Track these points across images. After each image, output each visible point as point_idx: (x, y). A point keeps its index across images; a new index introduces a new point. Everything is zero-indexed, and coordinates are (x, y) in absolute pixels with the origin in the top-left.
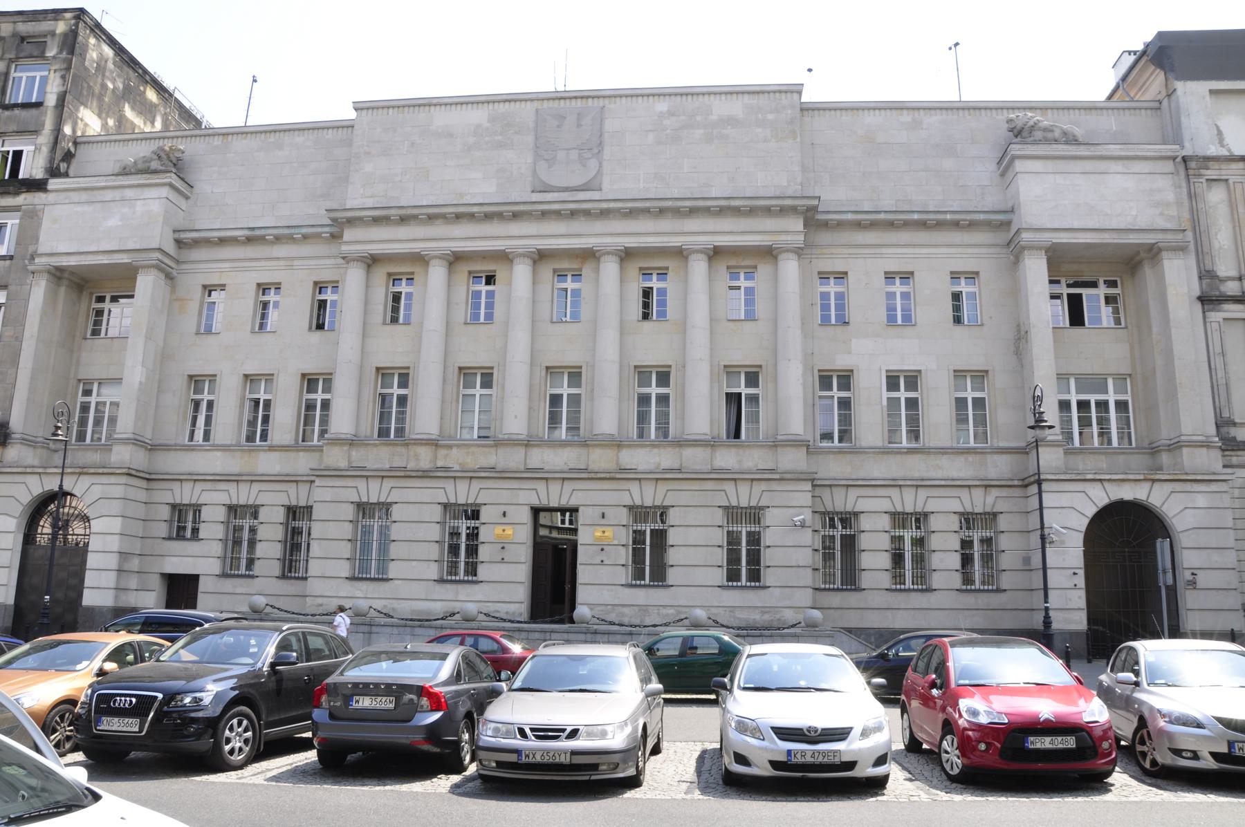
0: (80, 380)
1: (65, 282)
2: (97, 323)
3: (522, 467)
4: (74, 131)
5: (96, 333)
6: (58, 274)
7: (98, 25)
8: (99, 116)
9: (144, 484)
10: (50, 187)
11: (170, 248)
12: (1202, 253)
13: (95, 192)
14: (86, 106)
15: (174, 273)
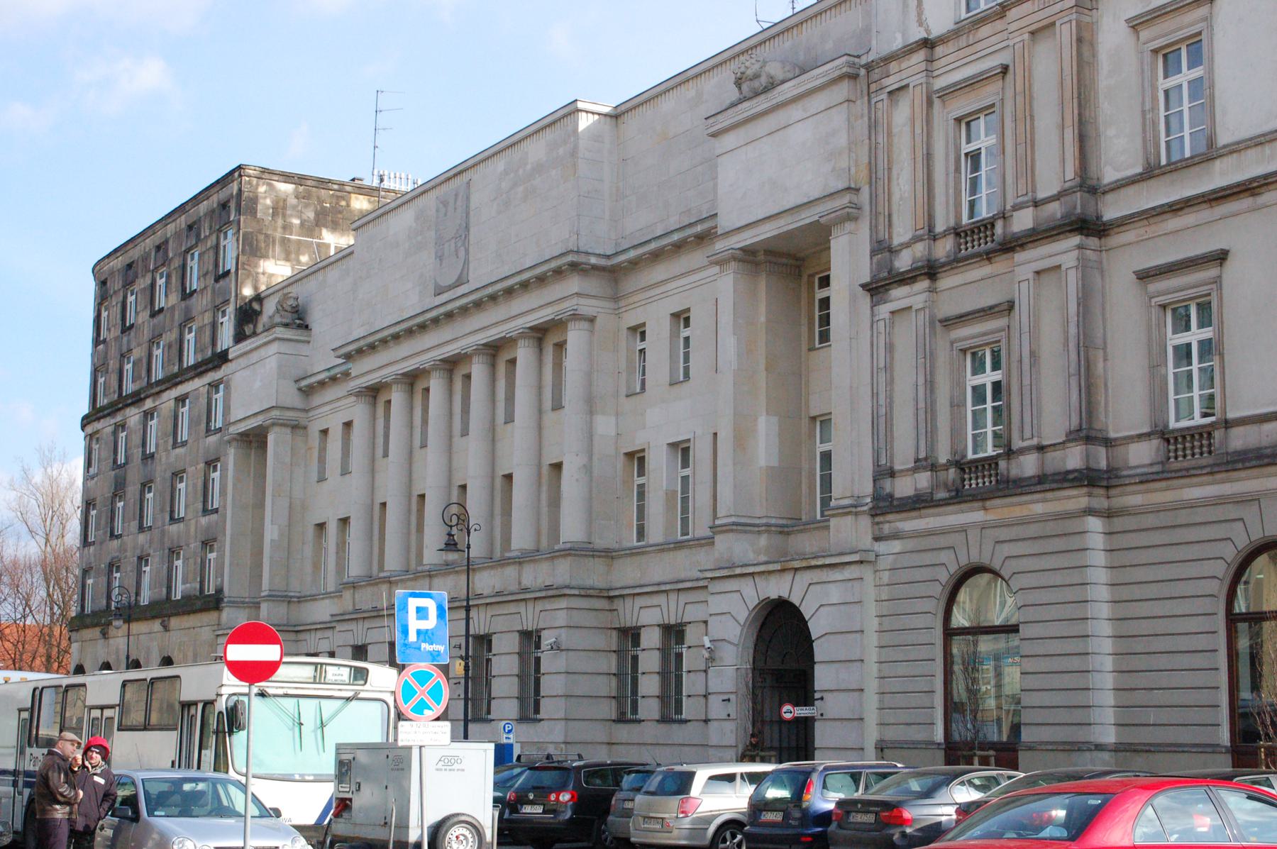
0: (814, 419)
1: (254, 445)
3: (514, 588)
4: (256, 288)
7: (265, 171)
8: (287, 259)
9: (603, 604)
11: (293, 398)
12: (882, 216)
13: (250, 356)
14: (265, 257)
15: (303, 423)
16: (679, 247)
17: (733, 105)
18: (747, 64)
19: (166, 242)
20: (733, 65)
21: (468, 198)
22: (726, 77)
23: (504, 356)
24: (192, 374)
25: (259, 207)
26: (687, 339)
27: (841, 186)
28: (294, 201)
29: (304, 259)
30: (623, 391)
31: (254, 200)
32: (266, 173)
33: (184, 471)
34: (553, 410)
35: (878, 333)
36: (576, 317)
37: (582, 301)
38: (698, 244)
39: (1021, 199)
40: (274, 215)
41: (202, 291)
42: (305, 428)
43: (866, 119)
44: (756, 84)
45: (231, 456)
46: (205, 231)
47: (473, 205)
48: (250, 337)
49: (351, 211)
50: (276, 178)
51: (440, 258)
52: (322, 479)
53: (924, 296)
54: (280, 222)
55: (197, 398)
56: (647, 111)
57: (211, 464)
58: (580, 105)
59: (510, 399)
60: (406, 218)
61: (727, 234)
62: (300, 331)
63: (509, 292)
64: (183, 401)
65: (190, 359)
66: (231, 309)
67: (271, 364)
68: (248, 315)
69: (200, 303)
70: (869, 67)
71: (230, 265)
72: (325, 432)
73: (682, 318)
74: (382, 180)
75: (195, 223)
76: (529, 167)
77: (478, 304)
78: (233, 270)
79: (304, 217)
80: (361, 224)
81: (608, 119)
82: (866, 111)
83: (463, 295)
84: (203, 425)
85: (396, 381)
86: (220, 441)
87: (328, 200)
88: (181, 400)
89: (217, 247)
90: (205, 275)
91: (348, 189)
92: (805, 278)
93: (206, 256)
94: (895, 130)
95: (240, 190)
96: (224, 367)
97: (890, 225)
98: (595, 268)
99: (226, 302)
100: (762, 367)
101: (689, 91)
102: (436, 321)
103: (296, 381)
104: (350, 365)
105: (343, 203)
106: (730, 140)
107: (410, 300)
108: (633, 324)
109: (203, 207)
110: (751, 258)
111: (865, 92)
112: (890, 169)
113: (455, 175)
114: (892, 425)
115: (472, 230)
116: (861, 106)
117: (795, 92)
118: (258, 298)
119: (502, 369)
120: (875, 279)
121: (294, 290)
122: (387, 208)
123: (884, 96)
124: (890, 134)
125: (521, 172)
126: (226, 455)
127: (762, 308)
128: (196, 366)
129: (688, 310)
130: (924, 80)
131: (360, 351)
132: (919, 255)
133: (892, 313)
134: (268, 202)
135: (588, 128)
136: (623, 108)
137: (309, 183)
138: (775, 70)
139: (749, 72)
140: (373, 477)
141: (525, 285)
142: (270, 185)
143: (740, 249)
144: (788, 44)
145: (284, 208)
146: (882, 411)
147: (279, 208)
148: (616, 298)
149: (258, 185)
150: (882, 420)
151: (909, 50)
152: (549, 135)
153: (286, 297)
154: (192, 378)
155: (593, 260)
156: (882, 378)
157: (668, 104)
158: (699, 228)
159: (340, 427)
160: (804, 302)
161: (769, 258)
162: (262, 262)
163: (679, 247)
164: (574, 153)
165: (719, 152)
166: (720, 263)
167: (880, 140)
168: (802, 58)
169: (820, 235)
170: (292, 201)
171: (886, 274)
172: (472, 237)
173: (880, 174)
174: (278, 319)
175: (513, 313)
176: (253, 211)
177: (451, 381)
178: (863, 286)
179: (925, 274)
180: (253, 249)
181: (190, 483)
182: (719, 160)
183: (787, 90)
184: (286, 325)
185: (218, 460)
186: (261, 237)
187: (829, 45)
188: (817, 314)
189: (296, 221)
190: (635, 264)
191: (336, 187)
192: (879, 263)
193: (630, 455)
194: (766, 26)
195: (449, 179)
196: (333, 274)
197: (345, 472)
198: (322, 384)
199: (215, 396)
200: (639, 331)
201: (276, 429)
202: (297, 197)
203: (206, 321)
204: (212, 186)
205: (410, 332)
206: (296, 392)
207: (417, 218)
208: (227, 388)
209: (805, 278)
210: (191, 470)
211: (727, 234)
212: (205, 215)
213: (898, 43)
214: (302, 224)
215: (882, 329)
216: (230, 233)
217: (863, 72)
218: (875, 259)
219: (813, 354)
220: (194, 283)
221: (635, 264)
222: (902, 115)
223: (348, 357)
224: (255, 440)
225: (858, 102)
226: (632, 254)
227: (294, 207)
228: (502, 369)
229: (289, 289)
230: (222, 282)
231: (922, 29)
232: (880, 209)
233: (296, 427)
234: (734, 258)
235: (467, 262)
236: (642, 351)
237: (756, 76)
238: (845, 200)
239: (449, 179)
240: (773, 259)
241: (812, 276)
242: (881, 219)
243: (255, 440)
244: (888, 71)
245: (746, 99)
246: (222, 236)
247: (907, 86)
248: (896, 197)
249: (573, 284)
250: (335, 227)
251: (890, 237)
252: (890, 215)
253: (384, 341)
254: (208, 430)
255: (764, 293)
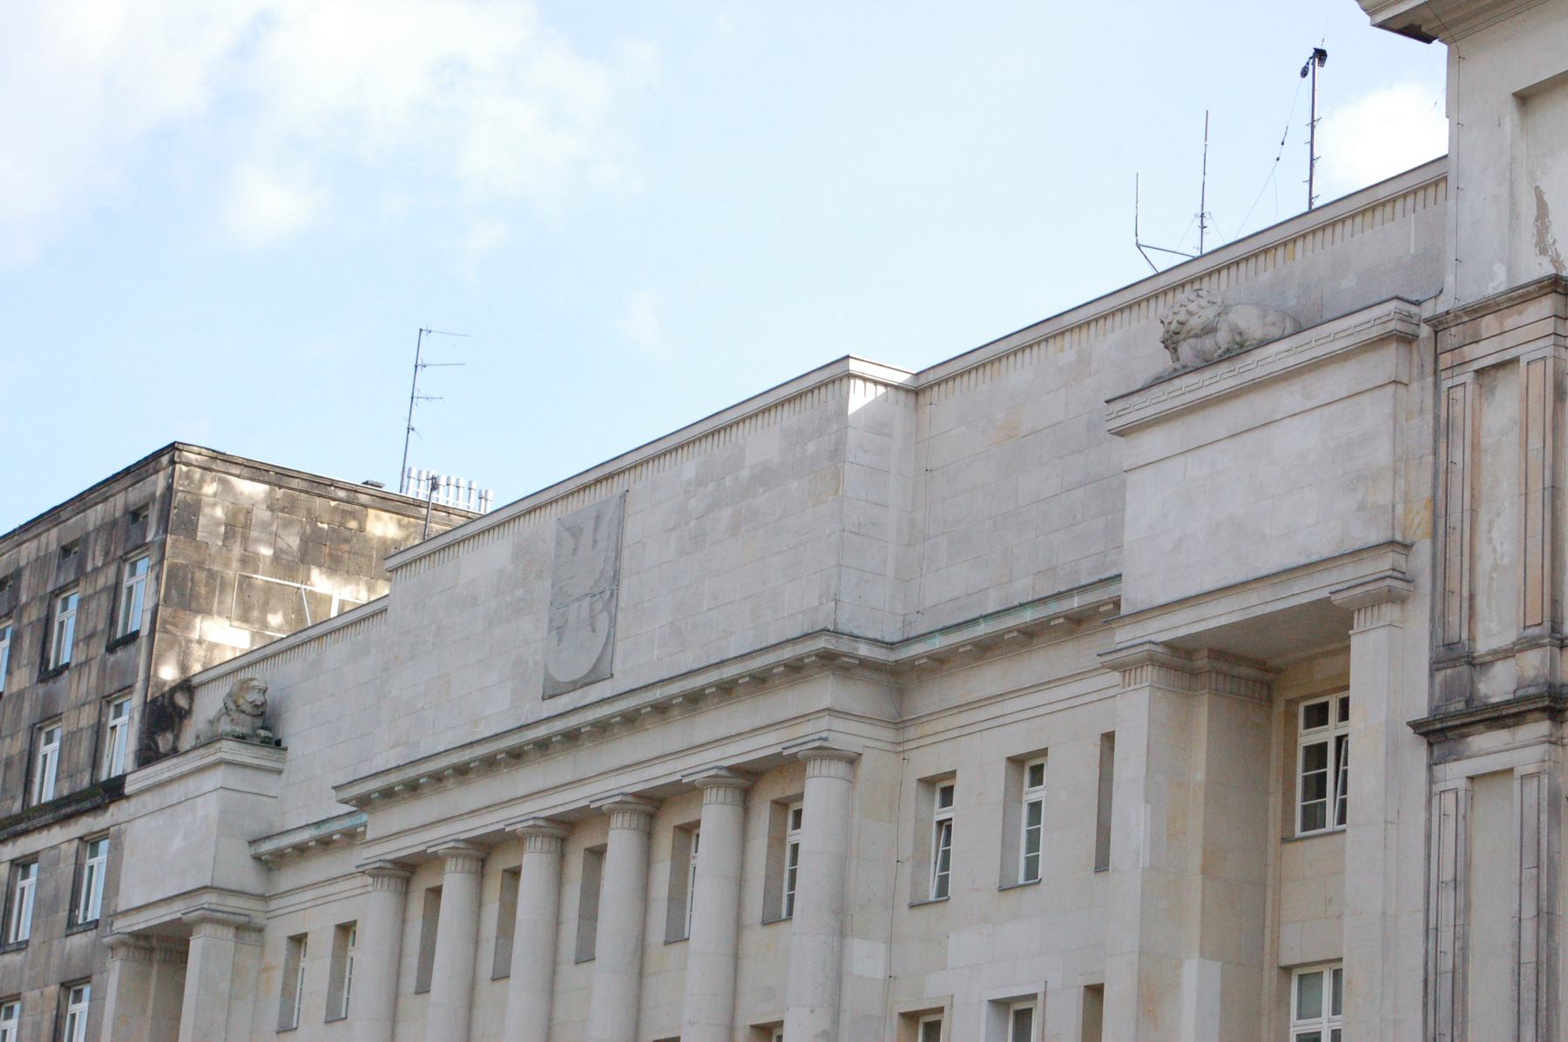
0: (1287, 970)
1: (158, 955)
2: (1316, 787)
4: (183, 667)
5: (1313, 819)
6: (142, 943)
7: (217, 456)
8: (245, 618)
10: (128, 790)
11: (243, 874)
12: (1453, 594)
14: (206, 612)
15: (259, 920)
16: (1030, 635)
17: (1158, 381)
18: (1192, 307)
19: (17, 574)
20: (1161, 308)
21: (621, 523)
22: (1147, 328)
23: (500, 863)
24: (48, 817)
25: (202, 521)
26: (1035, 807)
27: (1375, 537)
28: (267, 515)
29: (275, 619)
30: (905, 899)
31: (194, 508)
32: (219, 460)
33: (17, 997)
34: (765, 923)
35: (1443, 815)
36: (824, 752)
37: (838, 724)
38: (1070, 632)
39: (1530, 632)
40: (227, 537)
41: (80, 666)
42: (261, 930)
43: (1429, 418)
44: (1208, 343)
45: (114, 974)
46: (95, 558)
47: (629, 537)
48: (166, 756)
49: (366, 541)
50: (236, 470)
51: (559, 630)
52: (285, 1029)
53: (1536, 752)
54: (237, 550)
55: (55, 863)
56: (979, 385)
57: (71, 987)
58: (854, 366)
59: (589, 915)
60: (498, 552)
61: (1140, 615)
62: (265, 752)
63: (694, 700)
64: (94, 845)
65: (47, 789)
66: (133, 704)
67: (208, 808)
68: (164, 716)
69: (76, 689)
70: (1439, 324)
71: (139, 620)
72: (299, 940)
73: (1029, 766)
74: (434, 487)
75: (75, 543)
76: (745, 474)
77: (631, 720)
78: (145, 632)
79: (281, 544)
80: (392, 562)
81: (902, 395)
82: (1429, 402)
83: (603, 701)
84: (63, 915)
85: (454, 853)
86: (95, 945)
87: (326, 517)
88: (21, 865)
89: (116, 589)
90: (89, 638)
91: (363, 498)
92: (1280, 707)
93: (94, 604)
94: (1486, 441)
95: (170, 488)
96: (113, 809)
97: (1472, 616)
98: (865, 664)
99: (127, 689)
100: (1195, 861)
101: (1065, 352)
102: (543, 745)
103: (252, 842)
104: (364, 817)
105: (353, 524)
106: (1153, 443)
107: (494, 705)
108: (931, 772)
109: (95, 516)
110: (1187, 663)
111: (1429, 368)
112: (1474, 512)
113: (598, 481)
114: (1465, 991)
115: (624, 583)
116: (1420, 392)
117: (1291, 361)
118: (187, 686)
119: (665, 841)
120: (1436, 714)
121: (259, 675)
122: (459, 534)
123: (1468, 377)
124: (1476, 448)
125: (728, 481)
126: (104, 970)
127: (1200, 756)
128: (56, 804)
129: (1043, 752)
130: (1549, 352)
131: (388, 794)
132: (1530, 673)
133: (1471, 779)
134: (219, 512)
135: (865, 409)
136: (931, 377)
137: (295, 483)
138: (1248, 320)
139: (1195, 323)
140: (393, 1029)
141: (727, 690)
142: (223, 482)
143: (1166, 644)
144: (1264, 277)
145: (247, 526)
146: (1447, 964)
147: (238, 525)
148: (899, 724)
149: (202, 481)
150: (1446, 982)
151: (1520, 296)
152: (788, 418)
153: (245, 686)
154: (48, 826)
155: (863, 650)
156: (1448, 902)
157: (1018, 375)
158: (1076, 602)
159: (330, 933)
160: (1276, 750)
161: (1220, 665)
162: (198, 620)
163: (1030, 635)
164: (837, 452)
165: (1127, 465)
166: (1123, 668)
167: (1457, 456)
168: (1293, 303)
169: (1329, 628)
170: (262, 514)
171: (1461, 706)
172: (624, 599)
173: (1455, 519)
174: (225, 726)
175: (698, 740)
176: (189, 527)
177: (562, 857)
178: (1415, 725)
179: (1543, 710)
180: (184, 596)
181: (28, 1019)
182: (1130, 478)
183: (1276, 357)
184: (241, 738)
185: (87, 979)
186: (201, 576)
187: (1348, 282)
188: (1300, 774)
189: (266, 552)
190: (941, 662)
191: (342, 494)
192: (1447, 684)
193: (911, 1018)
194: (1163, 262)
195: (585, 488)
196: (336, 650)
197: (334, 1016)
198: (301, 850)
199: (89, 862)
200: (942, 788)
201: (207, 929)
202: (271, 508)
203: (84, 723)
204: (116, 478)
205: (490, 764)
206: (250, 863)
207: (516, 556)
208: (116, 848)
209: (1280, 707)
210: (31, 996)
211: (1140, 615)
212: (98, 530)
213: (1498, 282)
214: (276, 557)
215: (1451, 810)
216: (142, 566)
217: (1425, 331)
218: (1440, 676)
219: (1290, 847)
220: (65, 651)
221: (941, 662)
222: (1502, 415)
223: (364, 803)
224: (164, 948)
225: (1414, 387)
226: (938, 643)
227: (265, 526)
228: (665, 841)
229: (248, 674)
230: (121, 654)
231: (1545, 260)
232: (1453, 584)
233: (245, 928)
234: (1152, 660)
235: (610, 640)
236: (945, 826)
237: (1209, 330)
238: (1385, 562)
239: (585, 488)
240: (1225, 667)
241: (1292, 703)
242: (1454, 603)
243: (164, 948)
244: (1477, 331)
245: (1186, 371)
246: (127, 568)
247: (1514, 361)
248: (1485, 563)
249: (824, 691)
250: (335, 566)
251: (1472, 639)
252: (1472, 597)
253: (437, 778)
254: (71, 923)
255: (1205, 728)
